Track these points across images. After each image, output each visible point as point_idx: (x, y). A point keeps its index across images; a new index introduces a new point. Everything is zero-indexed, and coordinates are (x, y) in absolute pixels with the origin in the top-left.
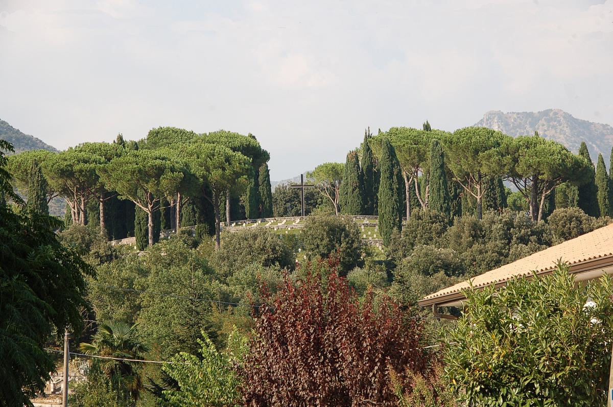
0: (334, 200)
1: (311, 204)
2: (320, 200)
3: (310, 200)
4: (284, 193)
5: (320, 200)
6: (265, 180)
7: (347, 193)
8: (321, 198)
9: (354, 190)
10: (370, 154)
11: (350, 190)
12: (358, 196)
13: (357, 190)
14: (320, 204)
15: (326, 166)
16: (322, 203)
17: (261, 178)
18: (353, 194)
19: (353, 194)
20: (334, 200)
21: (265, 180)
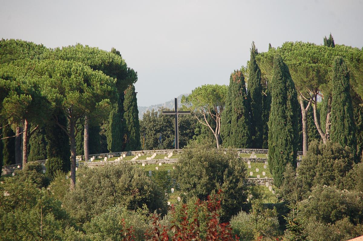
0: (214, 129)
1: (187, 135)
2: (197, 129)
3: (186, 129)
4: (154, 121)
5: (197, 129)
6: (131, 105)
7: (230, 122)
8: (199, 127)
9: (238, 118)
11: (234, 118)
12: (243, 125)
13: (243, 117)
14: (197, 135)
15: (205, 88)
17: (126, 103)
18: (237, 122)
19: (237, 122)
20: (214, 129)
21: (131, 105)
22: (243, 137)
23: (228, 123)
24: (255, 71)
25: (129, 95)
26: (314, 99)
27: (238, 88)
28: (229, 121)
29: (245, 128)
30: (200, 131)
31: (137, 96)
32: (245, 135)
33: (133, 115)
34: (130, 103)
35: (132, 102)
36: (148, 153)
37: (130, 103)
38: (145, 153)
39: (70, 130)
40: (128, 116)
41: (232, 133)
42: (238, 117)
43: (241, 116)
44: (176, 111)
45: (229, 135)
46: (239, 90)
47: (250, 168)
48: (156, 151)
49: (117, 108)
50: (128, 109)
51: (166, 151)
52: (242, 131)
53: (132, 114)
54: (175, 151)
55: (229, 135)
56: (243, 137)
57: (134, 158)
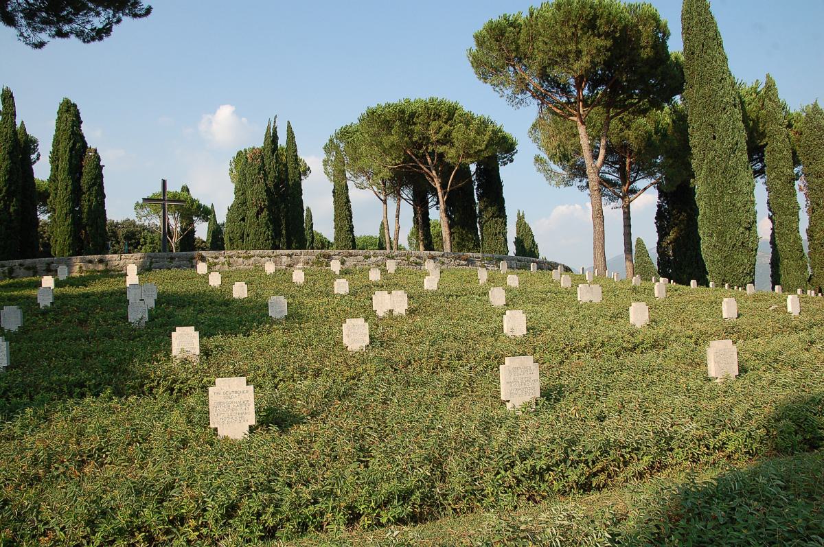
5: (143, 240)
6: (94, 184)
7: (243, 219)
9: (258, 213)
10: (276, 158)
11: (252, 212)
12: (267, 224)
13: (265, 212)
14: (142, 245)
16: (145, 244)
17: (85, 180)
18: (257, 218)
21: (94, 184)
22: (266, 240)
23: (240, 221)
24: (273, 153)
25: (92, 167)
26: (382, 198)
27: (257, 171)
28: (241, 217)
29: (268, 227)
30: (145, 241)
31: (104, 172)
32: (270, 237)
33: (97, 199)
34: (91, 180)
35: (96, 179)
36: (222, 259)
37: (91, 180)
38: (211, 260)
39: (626, 544)
40: (89, 201)
41: (248, 236)
42: (258, 211)
43: (261, 210)
44: (164, 199)
45: (242, 238)
46: (259, 173)
47: (521, 331)
48: (252, 252)
49: (70, 187)
50: (89, 188)
51: (290, 256)
52: (265, 232)
53: (96, 197)
54: (324, 256)
55: (242, 238)
56: (266, 240)
57: (335, 228)
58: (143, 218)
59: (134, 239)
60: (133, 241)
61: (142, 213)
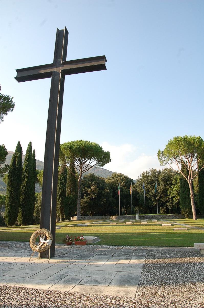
2: (174, 181)
4: (147, 177)
5: (174, 181)
8: (176, 180)
14: (174, 185)
15: (175, 138)
58: (165, 162)
59: (169, 181)
60: (168, 182)
61: (163, 159)
